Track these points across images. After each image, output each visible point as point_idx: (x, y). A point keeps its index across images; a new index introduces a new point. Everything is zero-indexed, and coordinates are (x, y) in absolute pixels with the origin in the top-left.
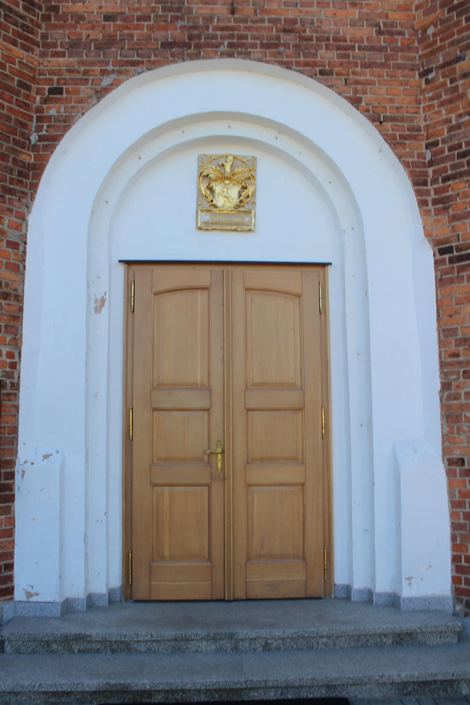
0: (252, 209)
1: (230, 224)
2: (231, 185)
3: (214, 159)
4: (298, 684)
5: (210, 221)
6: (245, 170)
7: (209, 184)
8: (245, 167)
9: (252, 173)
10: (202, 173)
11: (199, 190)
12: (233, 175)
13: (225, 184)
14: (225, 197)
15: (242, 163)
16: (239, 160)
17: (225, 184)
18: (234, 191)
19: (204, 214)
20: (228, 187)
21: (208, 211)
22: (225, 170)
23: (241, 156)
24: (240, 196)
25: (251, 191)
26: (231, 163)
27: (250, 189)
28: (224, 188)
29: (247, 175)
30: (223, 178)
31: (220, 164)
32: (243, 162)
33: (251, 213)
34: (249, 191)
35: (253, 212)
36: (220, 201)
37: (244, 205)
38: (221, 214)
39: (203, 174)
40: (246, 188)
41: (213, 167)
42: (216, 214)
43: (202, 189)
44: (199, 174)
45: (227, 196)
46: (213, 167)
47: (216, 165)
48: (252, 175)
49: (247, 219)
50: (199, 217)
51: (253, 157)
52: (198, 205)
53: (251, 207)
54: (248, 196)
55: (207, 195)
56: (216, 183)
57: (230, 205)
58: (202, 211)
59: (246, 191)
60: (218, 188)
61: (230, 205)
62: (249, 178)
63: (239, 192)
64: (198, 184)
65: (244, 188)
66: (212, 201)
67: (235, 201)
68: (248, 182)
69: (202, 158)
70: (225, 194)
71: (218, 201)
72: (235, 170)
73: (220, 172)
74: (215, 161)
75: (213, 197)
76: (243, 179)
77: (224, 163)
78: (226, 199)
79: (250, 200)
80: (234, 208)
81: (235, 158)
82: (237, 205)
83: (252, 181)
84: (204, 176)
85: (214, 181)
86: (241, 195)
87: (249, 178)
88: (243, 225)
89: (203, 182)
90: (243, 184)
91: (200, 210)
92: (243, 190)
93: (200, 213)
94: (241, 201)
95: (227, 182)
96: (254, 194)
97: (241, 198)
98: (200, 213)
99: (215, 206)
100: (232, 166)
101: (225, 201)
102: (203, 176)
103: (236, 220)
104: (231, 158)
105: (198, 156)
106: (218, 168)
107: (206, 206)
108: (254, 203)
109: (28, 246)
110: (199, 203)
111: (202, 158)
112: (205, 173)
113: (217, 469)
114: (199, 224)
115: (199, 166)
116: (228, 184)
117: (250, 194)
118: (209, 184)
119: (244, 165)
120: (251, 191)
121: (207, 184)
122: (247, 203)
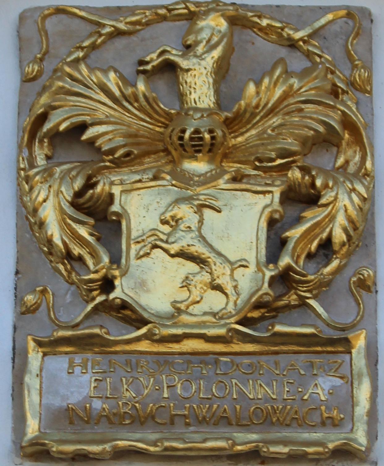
0: (353, 327)
1: (224, 420)
2: (222, 183)
3: (118, 33)
4: (46, 197)
5: (97, 404)
6: (306, 88)
7: (89, 185)
8: (304, 74)
9: (349, 105)
10: (43, 118)
11: (29, 222)
12: (234, 123)
13: (185, 180)
14: (183, 255)
15: (283, 52)
16: (265, 31)
17: (185, 180)
18: (239, 223)
19: (59, 363)
20: (204, 193)
21: (83, 343)
22: (181, 97)
23: (277, 10)
24: (276, 245)
25: (341, 219)
26: (216, 53)
27: (342, 205)
28: (177, 201)
29: (315, 119)
30: (167, 145)
31: (154, 59)
32: (292, 45)
33: (346, 344)
34: (332, 218)
35: (360, 343)
36: (155, 284)
37: (303, 304)
38: (163, 361)
39: (47, 126)
40: (312, 199)
41: (112, 81)
42: (133, 361)
43: (49, 213)
44: (27, 121)
45: (199, 249)
46: (112, 81)
47: (129, 71)
48: (348, 124)
49: (323, 387)
50: (31, 381)
51: (350, 15)
52: (25, 311)
53: (345, 313)
54: (327, 245)
55: (76, 250)
56: (128, 176)
57: (215, 301)
58: (49, 346)
59: (312, 216)
60: (142, 206)
61: (215, 301)
62: (328, 140)
63: (271, 223)
64: (24, 182)
65: (302, 198)
66: (107, 285)
67: (249, 281)
68: (323, 159)
69: (42, 31)
70: (185, 240)
71: (142, 285)
72: (243, 90)
73: (149, 107)
74: (120, 42)
75: (115, 260)
76: (291, 143)
77: (175, 56)
78: (192, 267)
79: (339, 270)
80: (243, 322)
81: (238, 21)
82: (258, 306)
83: (350, 155)
84: (55, 137)
85: (118, 164)
86: (284, 242)
87: (328, 140)
88: (301, 422)
89: (48, 173)
90: (295, 174)
91: (39, 344)
92: (292, 211)
93: (35, 358)
94: (285, 280)
95: (198, 166)
96: (360, 234)
97: (285, 260)
98: (35, 358)
99: (129, 314)
100: (222, 72)
101: (186, 284)
102: (53, 137)
103: (258, 391)
104: (214, 24)
105: (22, 18)
106: (141, 87)
107: (74, 312)
108: (364, 285)
109: (237, 3)
110: (30, 299)
111: (42, 31)
112: (59, 120)
113: (25, 71)
114: (33, 427)
115: (28, 80)
116: (207, 180)
117: (339, 236)
118: (89, 185)
119: (298, 63)
120: (341, 219)
121: (78, 184)
122: (322, 288)
